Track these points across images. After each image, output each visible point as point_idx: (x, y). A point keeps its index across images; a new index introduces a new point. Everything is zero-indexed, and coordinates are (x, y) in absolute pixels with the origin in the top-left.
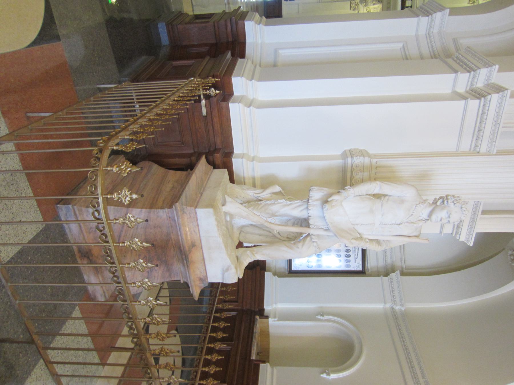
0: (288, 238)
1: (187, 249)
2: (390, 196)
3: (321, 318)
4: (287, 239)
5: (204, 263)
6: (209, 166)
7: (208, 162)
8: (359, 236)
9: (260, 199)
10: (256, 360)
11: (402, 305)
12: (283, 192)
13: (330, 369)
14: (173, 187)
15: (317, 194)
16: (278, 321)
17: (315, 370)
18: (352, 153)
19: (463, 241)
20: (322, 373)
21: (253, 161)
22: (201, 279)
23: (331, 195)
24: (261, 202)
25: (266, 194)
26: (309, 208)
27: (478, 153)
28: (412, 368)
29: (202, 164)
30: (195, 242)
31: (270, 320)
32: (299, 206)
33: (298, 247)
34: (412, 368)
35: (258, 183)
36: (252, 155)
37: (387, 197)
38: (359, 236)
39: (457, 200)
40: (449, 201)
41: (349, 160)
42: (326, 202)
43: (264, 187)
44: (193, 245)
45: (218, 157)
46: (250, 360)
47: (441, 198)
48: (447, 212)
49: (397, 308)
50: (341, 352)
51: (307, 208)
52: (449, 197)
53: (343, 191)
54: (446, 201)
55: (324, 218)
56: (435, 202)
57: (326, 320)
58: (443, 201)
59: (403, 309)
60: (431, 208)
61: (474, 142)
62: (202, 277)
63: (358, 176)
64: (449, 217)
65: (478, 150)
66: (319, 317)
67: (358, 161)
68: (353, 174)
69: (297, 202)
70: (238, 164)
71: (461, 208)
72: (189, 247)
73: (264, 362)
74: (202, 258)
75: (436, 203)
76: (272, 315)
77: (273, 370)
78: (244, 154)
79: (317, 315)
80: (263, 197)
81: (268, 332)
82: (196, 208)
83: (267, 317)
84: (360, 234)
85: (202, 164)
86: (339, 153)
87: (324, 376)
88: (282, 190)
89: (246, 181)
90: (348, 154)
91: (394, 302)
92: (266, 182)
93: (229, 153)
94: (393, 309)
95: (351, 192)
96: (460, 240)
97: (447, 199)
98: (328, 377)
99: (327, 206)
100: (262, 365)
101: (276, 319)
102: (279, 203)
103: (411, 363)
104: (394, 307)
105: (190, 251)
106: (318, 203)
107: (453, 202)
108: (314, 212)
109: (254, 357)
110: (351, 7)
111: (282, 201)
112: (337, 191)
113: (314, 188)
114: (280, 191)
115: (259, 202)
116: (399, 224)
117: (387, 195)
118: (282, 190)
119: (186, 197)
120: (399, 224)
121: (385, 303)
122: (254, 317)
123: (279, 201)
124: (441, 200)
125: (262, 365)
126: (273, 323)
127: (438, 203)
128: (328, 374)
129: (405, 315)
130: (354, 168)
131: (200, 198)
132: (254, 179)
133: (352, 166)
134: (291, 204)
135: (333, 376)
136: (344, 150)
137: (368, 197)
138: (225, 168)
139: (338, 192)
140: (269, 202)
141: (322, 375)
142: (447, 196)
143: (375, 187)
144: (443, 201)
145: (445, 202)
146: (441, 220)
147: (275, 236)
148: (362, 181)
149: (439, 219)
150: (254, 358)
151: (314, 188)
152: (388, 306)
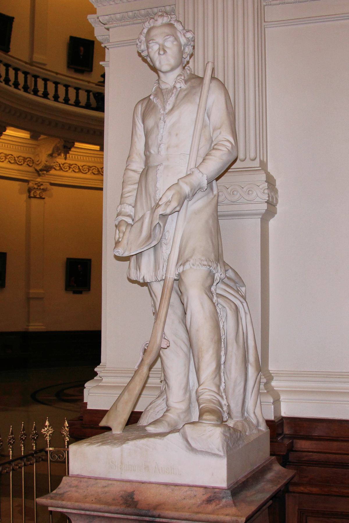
5: (176, 485)
22: (209, 501)
62: (205, 497)
110: (41, 198)
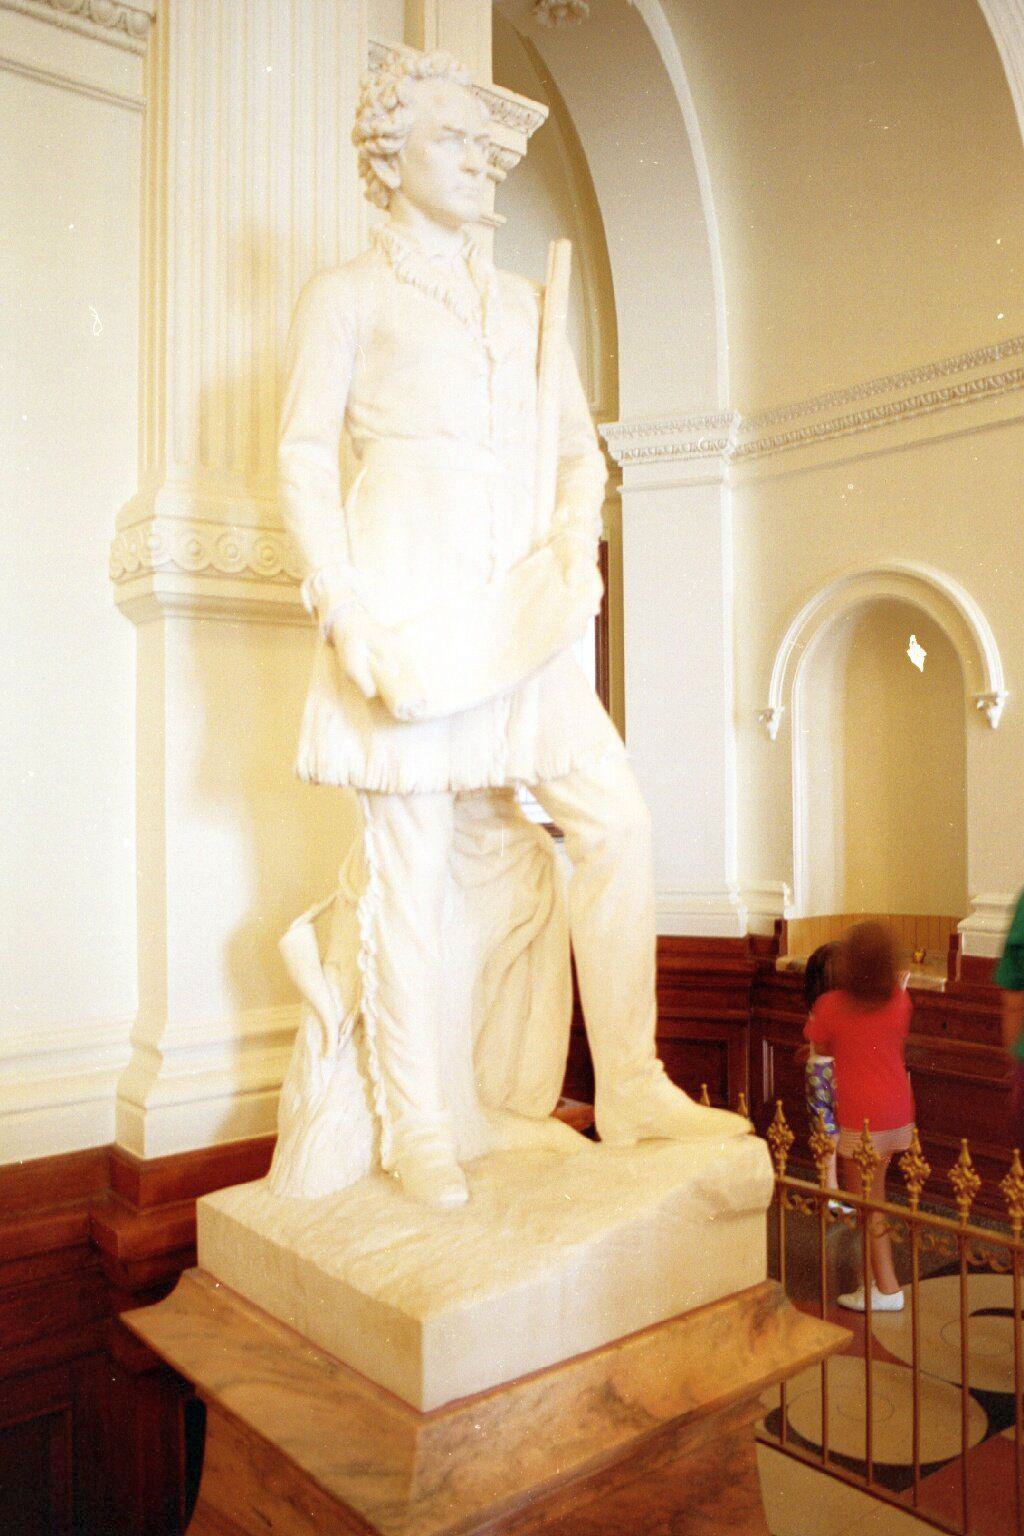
0: (540, 884)
1: (628, 1435)
2: (350, 395)
3: (776, 717)
4: (547, 885)
6: (182, 1291)
7: (156, 1290)
8: (546, 553)
9: (350, 1025)
10: (951, 973)
11: (726, 421)
12: (315, 909)
13: (971, 691)
14: (291, 1501)
15: (334, 746)
16: (792, 886)
17: (975, 743)
18: (133, 572)
19: (531, 143)
20: (988, 722)
21: (157, 1054)
23: (344, 682)
24: (369, 1021)
25: (325, 993)
26: (406, 787)
27: (153, 20)
28: (954, 395)
29: (160, 1327)
30: (591, 1389)
31: (792, 913)
32: (391, 828)
33: (600, 846)
34: (954, 395)
35: (267, 1019)
36: (129, 1051)
37: (359, 412)
38: (546, 553)
39: (382, 95)
40: (385, 126)
41: (169, 585)
42: (379, 703)
43: (289, 992)
44: (607, 1397)
45: (132, 1232)
46: (951, 993)
47: (365, 166)
48: (439, 141)
49: (735, 439)
50: (900, 644)
51: (406, 797)
52: (367, 129)
53: (323, 620)
54: (382, 142)
55: (456, 717)
56: (386, 197)
57: (787, 698)
58: (385, 157)
59: (738, 419)
60: (416, 216)
61: (100, 30)
62: (746, 1323)
63: (243, 546)
64: (460, 134)
65: (140, 19)
66: (774, 726)
67: (170, 542)
68: (230, 570)
69: (375, 843)
70: (177, 1126)
71: (419, 77)
72: (620, 1422)
73: (955, 941)
74: (662, 1334)
75: (388, 190)
76: (771, 906)
77: (982, 907)
78: (120, 1097)
79: (768, 734)
80: (340, 1009)
81: (831, 919)
82: (414, 1411)
83: (780, 925)
84: (535, 548)
85: (160, 1327)
86: (128, 634)
87: (996, 714)
88: (308, 915)
89: (257, 1077)
90: (136, 588)
91: (715, 449)
92: (259, 972)
93: (110, 1171)
94: (736, 456)
95: (334, 580)
96: (524, 152)
97: (374, 137)
98: (1001, 702)
99: (401, 700)
100: (966, 948)
101: (787, 891)
102: (377, 932)
103: (874, 418)
104: (733, 451)
105: (633, 1414)
106: (384, 741)
107: (390, 110)
108: (423, 762)
109: (940, 981)
111: (365, 918)
112: (321, 651)
113: (303, 764)
114: (314, 920)
115: (371, 1030)
116: (491, 359)
117: (348, 412)
118: (308, 915)
119: (358, 1470)
120: (491, 359)
121: (720, 481)
122: (783, 975)
123: (365, 935)
124: (380, 168)
125: (966, 948)
126: (799, 898)
127: (392, 179)
128: (992, 699)
129: (761, 418)
130: (203, 564)
131: (358, 1375)
132: (246, 1042)
133: (198, 574)
134: (382, 876)
135: (997, 681)
136: (116, 610)
137: (353, 497)
138: (194, 1205)
139: (331, 642)
140: (371, 982)
141: (995, 724)
142: (360, 139)
143: (307, 462)
144: (385, 157)
145: (389, 145)
146: (472, 171)
147: (530, 946)
148: (275, 527)
149: (466, 178)
150: (944, 980)
151: (303, 764)
152: (727, 470)
